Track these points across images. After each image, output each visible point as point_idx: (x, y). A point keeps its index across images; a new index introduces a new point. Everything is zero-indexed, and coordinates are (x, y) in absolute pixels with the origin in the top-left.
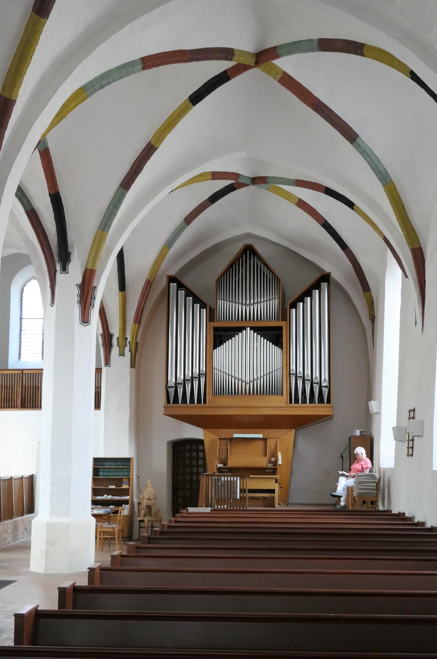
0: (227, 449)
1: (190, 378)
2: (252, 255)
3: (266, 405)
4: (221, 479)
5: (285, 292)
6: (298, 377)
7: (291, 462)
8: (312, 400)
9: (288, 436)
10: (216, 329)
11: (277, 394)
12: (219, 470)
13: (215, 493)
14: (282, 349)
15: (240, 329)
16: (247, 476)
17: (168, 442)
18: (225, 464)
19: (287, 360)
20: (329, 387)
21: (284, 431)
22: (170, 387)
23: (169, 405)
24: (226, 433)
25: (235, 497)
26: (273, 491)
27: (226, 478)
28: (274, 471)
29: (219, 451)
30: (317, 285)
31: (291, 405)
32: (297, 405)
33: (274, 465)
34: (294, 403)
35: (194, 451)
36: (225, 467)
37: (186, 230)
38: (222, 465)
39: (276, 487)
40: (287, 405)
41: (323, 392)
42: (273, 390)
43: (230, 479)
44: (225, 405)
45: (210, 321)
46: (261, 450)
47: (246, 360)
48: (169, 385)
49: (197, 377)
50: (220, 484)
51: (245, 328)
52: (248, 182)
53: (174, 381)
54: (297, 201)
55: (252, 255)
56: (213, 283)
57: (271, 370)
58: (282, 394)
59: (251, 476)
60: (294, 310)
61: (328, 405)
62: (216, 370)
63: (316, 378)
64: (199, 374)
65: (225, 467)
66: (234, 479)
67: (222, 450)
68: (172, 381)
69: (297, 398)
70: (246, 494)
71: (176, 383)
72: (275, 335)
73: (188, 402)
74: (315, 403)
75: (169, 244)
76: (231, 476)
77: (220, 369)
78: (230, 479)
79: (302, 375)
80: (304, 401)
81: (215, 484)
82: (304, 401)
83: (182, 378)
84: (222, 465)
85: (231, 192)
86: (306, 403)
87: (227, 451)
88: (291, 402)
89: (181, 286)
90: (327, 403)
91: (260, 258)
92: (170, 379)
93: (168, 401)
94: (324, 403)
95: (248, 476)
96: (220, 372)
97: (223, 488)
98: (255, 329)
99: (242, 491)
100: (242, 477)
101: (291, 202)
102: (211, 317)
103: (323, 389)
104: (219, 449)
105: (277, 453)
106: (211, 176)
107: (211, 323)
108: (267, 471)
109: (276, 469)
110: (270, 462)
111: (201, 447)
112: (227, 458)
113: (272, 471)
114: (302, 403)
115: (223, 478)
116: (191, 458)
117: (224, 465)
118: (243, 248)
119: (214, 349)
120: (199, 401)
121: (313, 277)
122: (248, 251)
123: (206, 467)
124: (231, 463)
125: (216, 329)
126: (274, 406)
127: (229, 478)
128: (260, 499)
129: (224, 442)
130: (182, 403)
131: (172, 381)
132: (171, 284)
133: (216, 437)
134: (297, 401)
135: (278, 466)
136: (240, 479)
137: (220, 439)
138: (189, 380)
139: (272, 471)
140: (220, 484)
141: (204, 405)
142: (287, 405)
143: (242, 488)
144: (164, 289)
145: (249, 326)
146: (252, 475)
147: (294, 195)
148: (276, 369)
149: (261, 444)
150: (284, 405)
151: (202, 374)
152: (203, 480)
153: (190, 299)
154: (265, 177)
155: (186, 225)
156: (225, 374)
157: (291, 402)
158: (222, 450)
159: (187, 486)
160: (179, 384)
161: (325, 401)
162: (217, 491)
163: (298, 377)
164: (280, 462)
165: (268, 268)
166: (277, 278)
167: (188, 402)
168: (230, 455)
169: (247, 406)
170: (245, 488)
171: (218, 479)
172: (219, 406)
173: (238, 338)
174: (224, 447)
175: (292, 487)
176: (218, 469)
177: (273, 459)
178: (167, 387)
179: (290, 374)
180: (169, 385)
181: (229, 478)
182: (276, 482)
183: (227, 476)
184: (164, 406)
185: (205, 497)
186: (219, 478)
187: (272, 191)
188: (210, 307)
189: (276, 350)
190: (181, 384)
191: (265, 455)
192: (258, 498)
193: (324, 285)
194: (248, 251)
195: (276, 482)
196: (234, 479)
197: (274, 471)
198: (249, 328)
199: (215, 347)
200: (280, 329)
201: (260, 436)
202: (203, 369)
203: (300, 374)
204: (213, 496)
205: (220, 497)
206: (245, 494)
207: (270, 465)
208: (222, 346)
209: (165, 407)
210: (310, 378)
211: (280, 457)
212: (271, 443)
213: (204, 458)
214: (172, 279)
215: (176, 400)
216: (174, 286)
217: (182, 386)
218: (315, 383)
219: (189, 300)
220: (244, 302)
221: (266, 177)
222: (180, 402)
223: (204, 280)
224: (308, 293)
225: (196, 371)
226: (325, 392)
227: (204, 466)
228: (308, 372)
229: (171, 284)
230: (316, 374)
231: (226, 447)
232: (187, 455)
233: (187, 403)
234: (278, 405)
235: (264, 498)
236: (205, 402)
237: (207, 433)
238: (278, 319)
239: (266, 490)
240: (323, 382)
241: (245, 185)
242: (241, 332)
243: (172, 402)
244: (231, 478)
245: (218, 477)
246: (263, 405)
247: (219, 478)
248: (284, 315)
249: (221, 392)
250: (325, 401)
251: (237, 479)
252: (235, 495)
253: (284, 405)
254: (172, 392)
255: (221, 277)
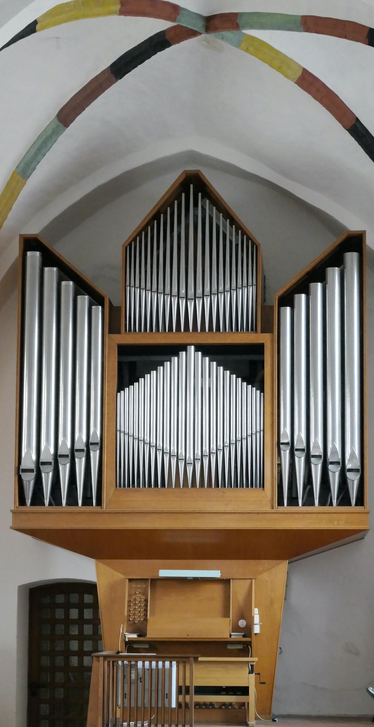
0: (146, 601)
1: (68, 452)
2: (200, 194)
3: (229, 509)
4: (136, 665)
5: (265, 277)
6: (297, 450)
7: (272, 627)
8: (325, 500)
9: (275, 574)
10: (123, 350)
11: (252, 486)
12: (130, 645)
13: (124, 696)
14: (262, 390)
15: (174, 350)
16: (192, 659)
17: (21, 588)
18: (142, 634)
19: (273, 414)
20: (361, 471)
21: (266, 563)
22: (25, 471)
23: (23, 508)
24: (141, 567)
25: (167, 705)
26: (244, 691)
27: (147, 663)
28: (245, 649)
29: (129, 606)
30: (336, 259)
31: (281, 509)
32: (293, 509)
33: (244, 636)
34: (288, 505)
35: (74, 606)
36: (141, 639)
37: (61, 139)
38: (134, 636)
39: (250, 681)
40: (273, 508)
41: (349, 482)
42: (245, 477)
43: (157, 666)
44: (144, 509)
45: (110, 332)
46: (218, 604)
47: (186, 413)
48: (24, 466)
49: (83, 450)
50: (133, 676)
51: (184, 347)
52: (198, 26)
53: (34, 457)
54: (299, 74)
55: (200, 194)
56: (115, 255)
57: (239, 436)
58: (262, 485)
59: (200, 659)
60: (288, 309)
61: (360, 509)
62: (122, 435)
63: (334, 452)
64: (88, 444)
65: (141, 639)
66: (164, 666)
67: (135, 604)
68: (29, 457)
69: (294, 496)
70: (191, 698)
71: (38, 463)
72: (247, 363)
73: (64, 502)
74: (331, 504)
75: (25, 169)
76: (157, 659)
77: (131, 433)
78: (157, 666)
79: (304, 446)
80: (309, 501)
81: (124, 677)
82: (309, 501)
83: (52, 451)
84: (134, 636)
85: (160, 50)
86: (312, 504)
87: (146, 606)
88: (281, 503)
89: (50, 258)
90: (356, 504)
91: (216, 202)
92: (26, 454)
93: (22, 501)
94: (349, 504)
95: (196, 659)
96: (131, 439)
97: (140, 685)
98: (207, 350)
99: (182, 690)
100: (182, 661)
101: (287, 77)
102: (113, 324)
103: (349, 475)
104: (129, 601)
105: (251, 610)
106: (118, 7)
107: (112, 335)
108: (229, 647)
109: (249, 644)
110: (236, 628)
111: (88, 599)
112: (146, 620)
113: (240, 647)
114: (304, 505)
115: (140, 664)
116: (68, 621)
117: (139, 636)
118: (182, 179)
119: (119, 391)
120: (87, 501)
121: (325, 245)
122: (192, 186)
123: (100, 638)
124: (155, 631)
125: (123, 350)
126: (245, 510)
127: (154, 663)
128: (216, 706)
129: (139, 586)
130: (50, 504)
131: (29, 457)
132: (29, 253)
133: (123, 576)
134: (293, 501)
135: (253, 635)
136: (178, 666)
137: (130, 580)
138: (67, 456)
139: (240, 647)
140: (133, 676)
141: (98, 509)
142: (273, 508)
143: (181, 684)
144: (13, 268)
145: (193, 342)
146: (202, 656)
147: (292, 60)
148: (249, 432)
149: (217, 590)
150: (268, 509)
151: (92, 444)
152: (99, 670)
153: (69, 286)
154: (235, 15)
155: (61, 125)
156: (141, 444)
157: (281, 503)
158: (135, 604)
159: (60, 677)
160: (44, 463)
161: (353, 501)
162: (127, 691)
163: (297, 450)
164: (257, 629)
165: (233, 221)
166: (253, 243)
167: (64, 502)
168: (153, 613)
169: (189, 510)
170: (188, 684)
171: (131, 666)
172: (128, 510)
173: (171, 368)
174: (139, 597)
175: (279, 681)
176: (126, 643)
177: (242, 623)
178: (19, 471)
179: (279, 443)
180: (24, 466)
181: (154, 663)
182: (251, 672)
183: (150, 659)
184: (11, 511)
185: (100, 706)
186: (133, 663)
187: (247, 50)
188: (110, 303)
189: (251, 393)
190: (50, 463)
191: (226, 614)
192: (211, 704)
193: (352, 258)
194: (192, 186)
195: (251, 672)
196: (164, 666)
197: (245, 649)
198: (193, 347)
199: (121, 387)
200: (259, 349)
201: (216, 574)
202: (95, 432)
203: (300, 443)
204: (120, 702)
205: (133, 705)
206: (188, 698)
207: (237, 636)
208: (136, 384)
209: (14, 512)
210: (320, 452)
211: (257, 619)
212: (238, 590)
213: (96, 622)
214: (30, 243)
215: (38, 499)
216: (34, 257)
217: (51, 468)
218: (332, 463)
219: (67, 286)
220: (183, 291)
221: (236, 15)
222: (47, 502)
223: (99, 250)
224: (318, 274)
225: (80, 437)
226: (353, 481)
227: (96, 637)
228: (317, 440)
229: (29, 253)
230: (334, 444)
231: (143, 598)
232: (60, 614)
233: (61, 505)
234: (252, 509)
235: (224, 704)
236: (99, 503)
237: (103, 567)
238: (254, 329)
239: (227, 687)
240: (349, 460)
241: (193, 33)
242: (177, 355)
243: (29, 502)
244: (157, 662)
245: (130, 662)
246: (222, 509)
247: (133, 663)
248: (267, 320)
249: (132, 481)
250: (353, 501)
251: (171, 665)
252: (166, 701)
253: (268, 509)
254: (29, 481)
255: (135, 240)
